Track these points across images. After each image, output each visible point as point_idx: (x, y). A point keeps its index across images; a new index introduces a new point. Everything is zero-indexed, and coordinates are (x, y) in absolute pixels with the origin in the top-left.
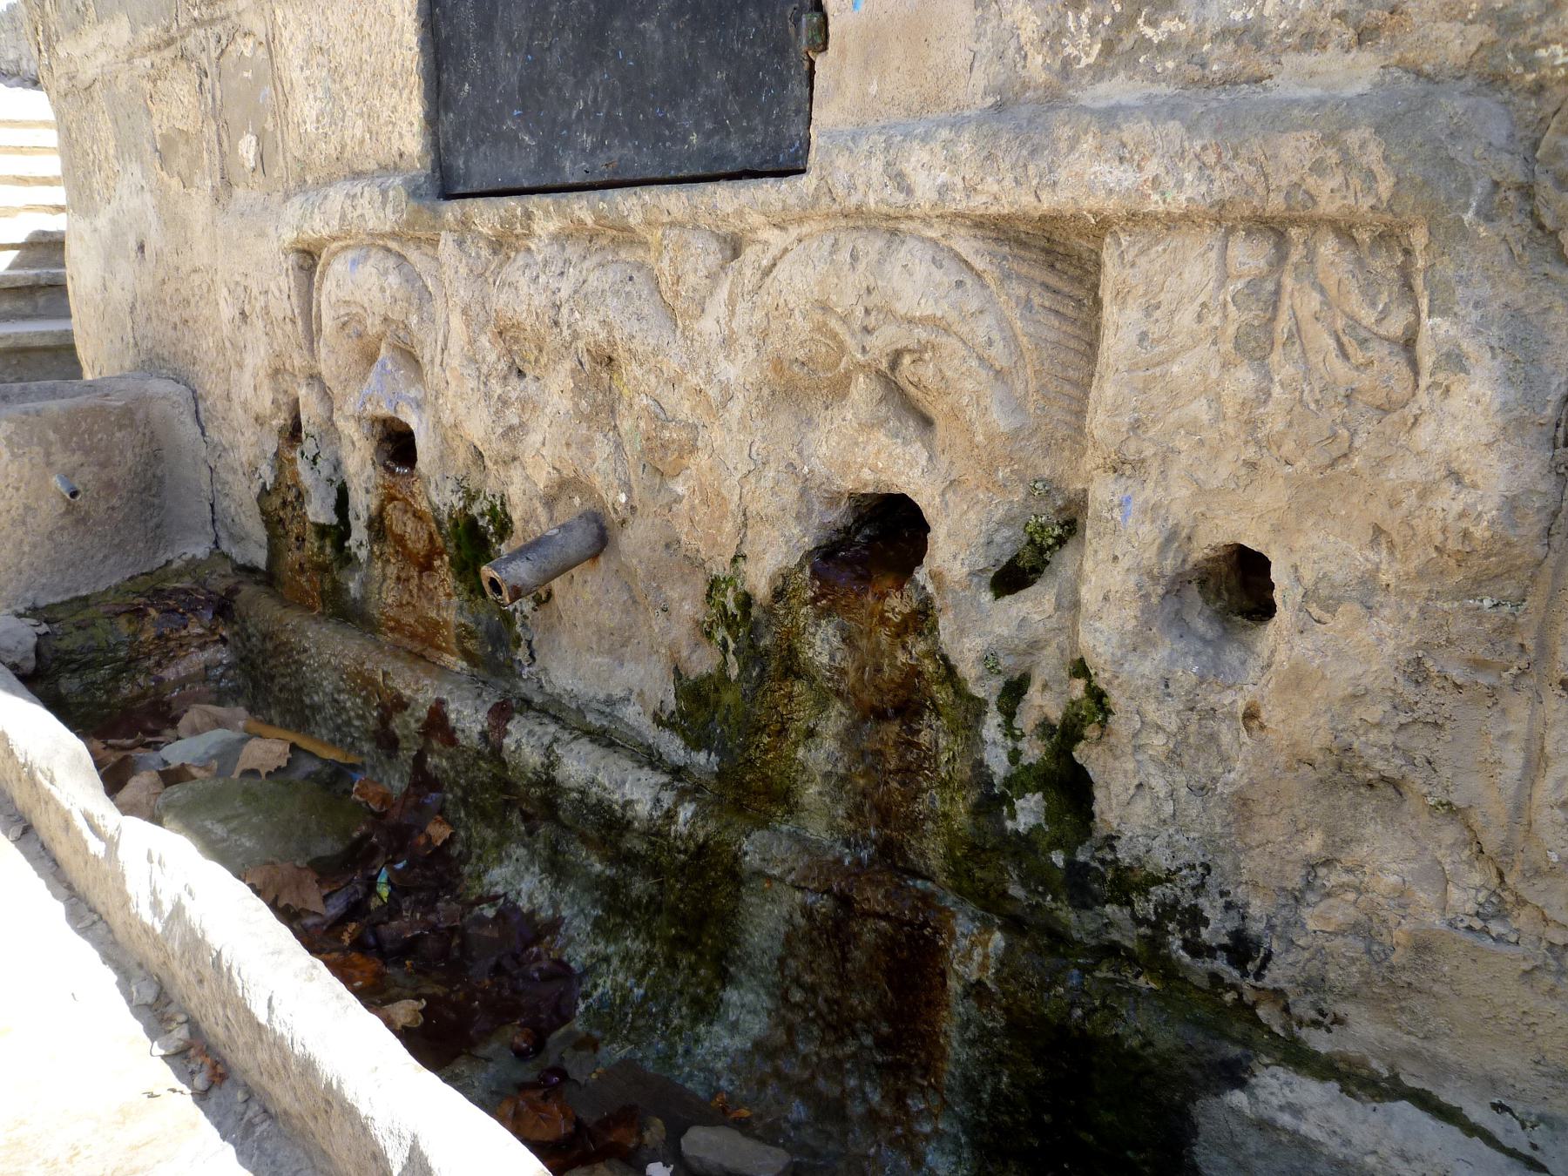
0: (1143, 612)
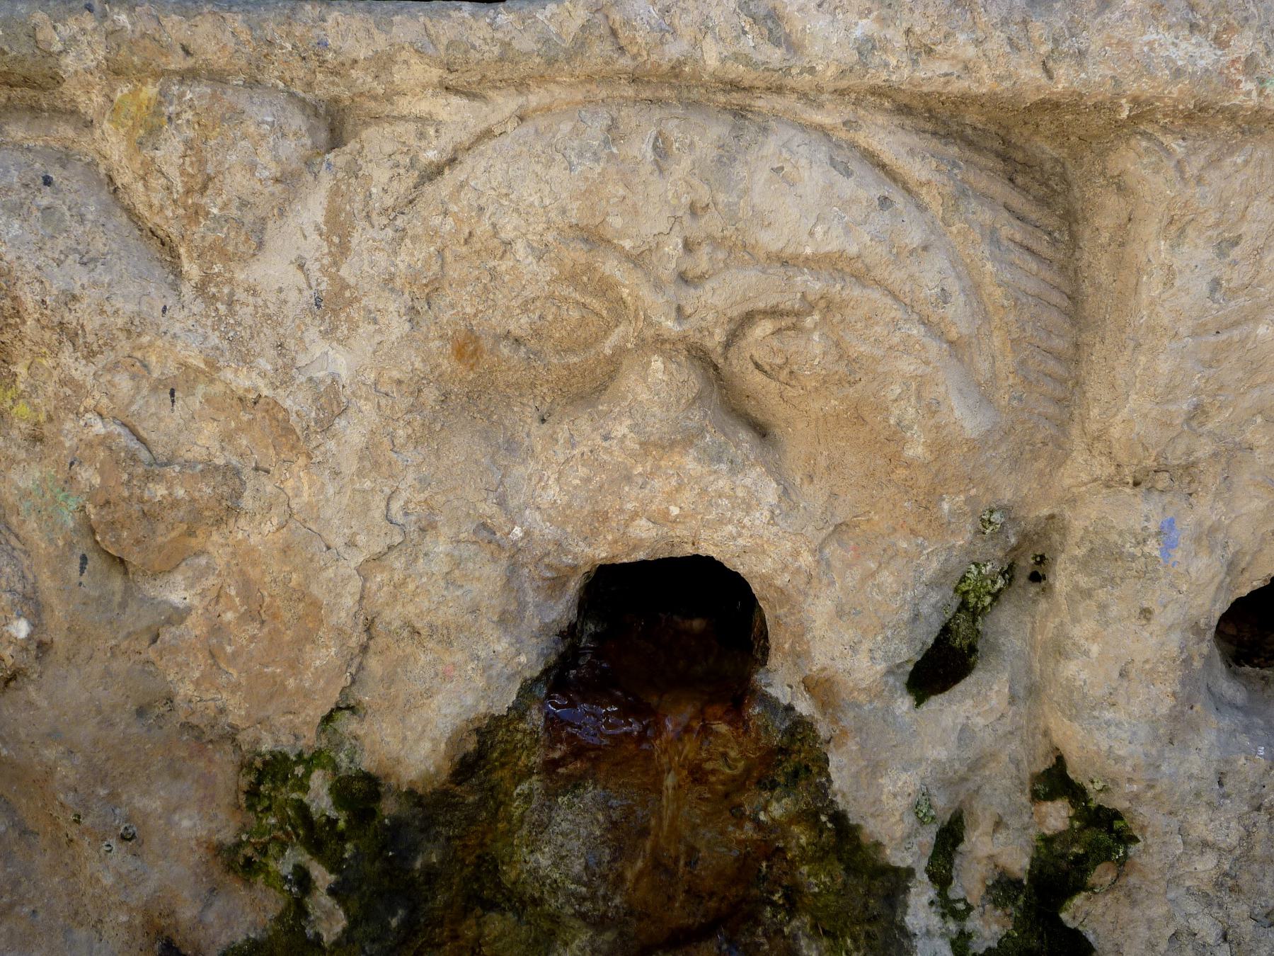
0: (1183, 684)
